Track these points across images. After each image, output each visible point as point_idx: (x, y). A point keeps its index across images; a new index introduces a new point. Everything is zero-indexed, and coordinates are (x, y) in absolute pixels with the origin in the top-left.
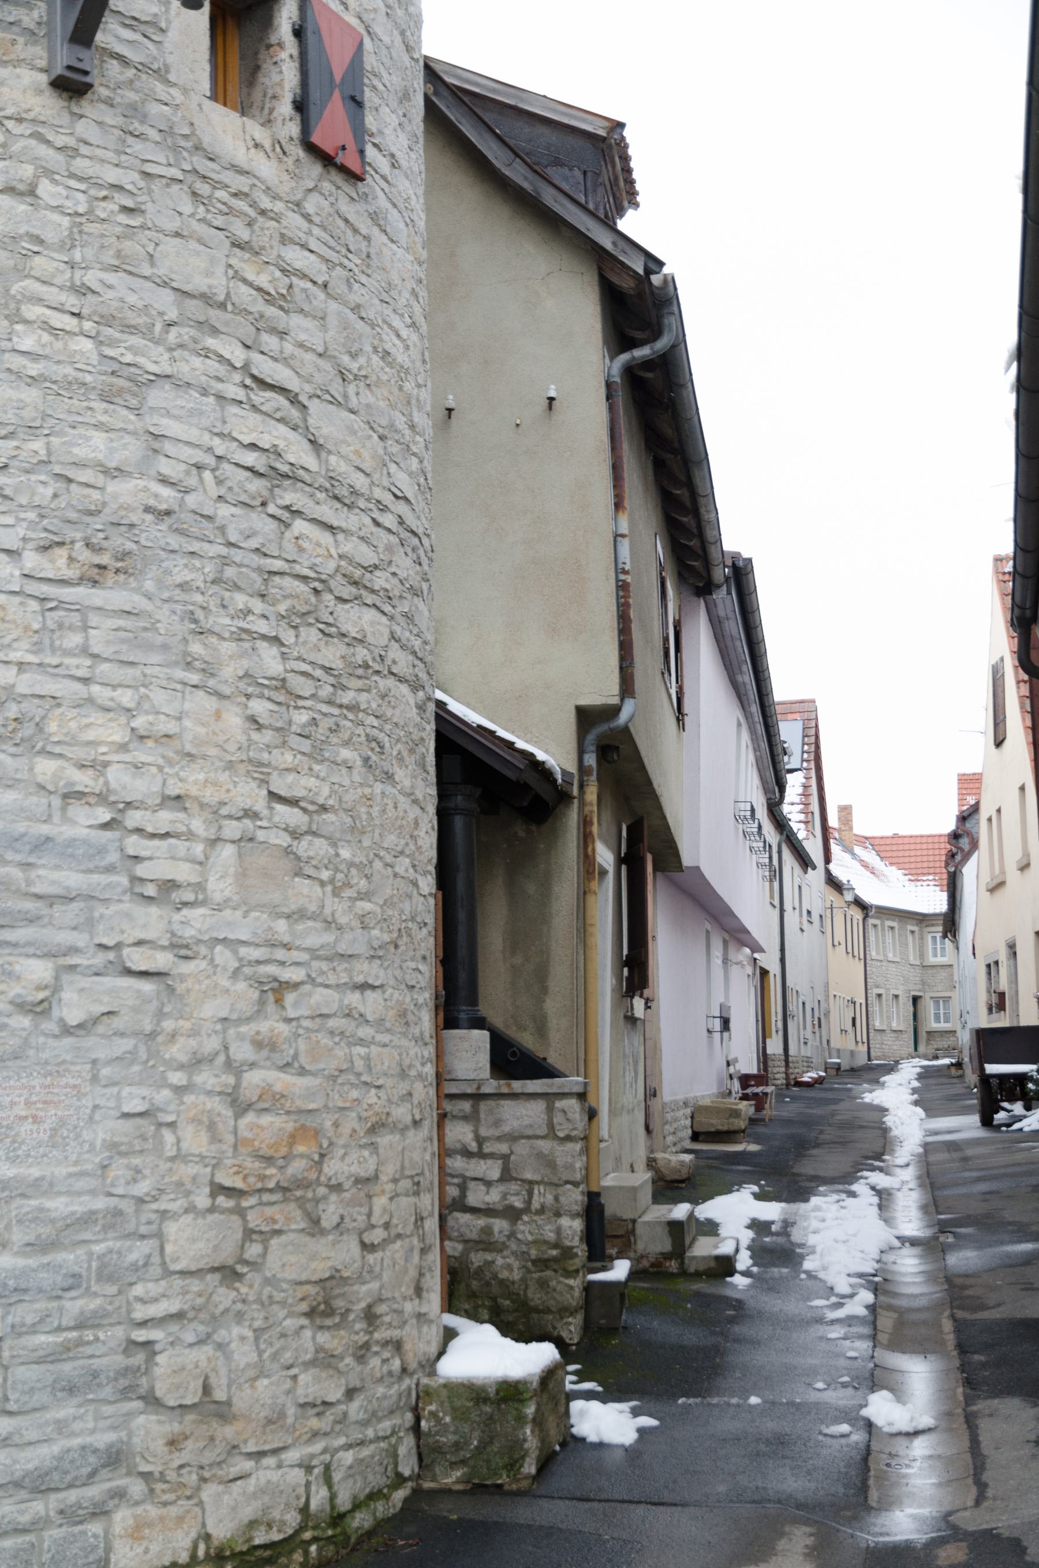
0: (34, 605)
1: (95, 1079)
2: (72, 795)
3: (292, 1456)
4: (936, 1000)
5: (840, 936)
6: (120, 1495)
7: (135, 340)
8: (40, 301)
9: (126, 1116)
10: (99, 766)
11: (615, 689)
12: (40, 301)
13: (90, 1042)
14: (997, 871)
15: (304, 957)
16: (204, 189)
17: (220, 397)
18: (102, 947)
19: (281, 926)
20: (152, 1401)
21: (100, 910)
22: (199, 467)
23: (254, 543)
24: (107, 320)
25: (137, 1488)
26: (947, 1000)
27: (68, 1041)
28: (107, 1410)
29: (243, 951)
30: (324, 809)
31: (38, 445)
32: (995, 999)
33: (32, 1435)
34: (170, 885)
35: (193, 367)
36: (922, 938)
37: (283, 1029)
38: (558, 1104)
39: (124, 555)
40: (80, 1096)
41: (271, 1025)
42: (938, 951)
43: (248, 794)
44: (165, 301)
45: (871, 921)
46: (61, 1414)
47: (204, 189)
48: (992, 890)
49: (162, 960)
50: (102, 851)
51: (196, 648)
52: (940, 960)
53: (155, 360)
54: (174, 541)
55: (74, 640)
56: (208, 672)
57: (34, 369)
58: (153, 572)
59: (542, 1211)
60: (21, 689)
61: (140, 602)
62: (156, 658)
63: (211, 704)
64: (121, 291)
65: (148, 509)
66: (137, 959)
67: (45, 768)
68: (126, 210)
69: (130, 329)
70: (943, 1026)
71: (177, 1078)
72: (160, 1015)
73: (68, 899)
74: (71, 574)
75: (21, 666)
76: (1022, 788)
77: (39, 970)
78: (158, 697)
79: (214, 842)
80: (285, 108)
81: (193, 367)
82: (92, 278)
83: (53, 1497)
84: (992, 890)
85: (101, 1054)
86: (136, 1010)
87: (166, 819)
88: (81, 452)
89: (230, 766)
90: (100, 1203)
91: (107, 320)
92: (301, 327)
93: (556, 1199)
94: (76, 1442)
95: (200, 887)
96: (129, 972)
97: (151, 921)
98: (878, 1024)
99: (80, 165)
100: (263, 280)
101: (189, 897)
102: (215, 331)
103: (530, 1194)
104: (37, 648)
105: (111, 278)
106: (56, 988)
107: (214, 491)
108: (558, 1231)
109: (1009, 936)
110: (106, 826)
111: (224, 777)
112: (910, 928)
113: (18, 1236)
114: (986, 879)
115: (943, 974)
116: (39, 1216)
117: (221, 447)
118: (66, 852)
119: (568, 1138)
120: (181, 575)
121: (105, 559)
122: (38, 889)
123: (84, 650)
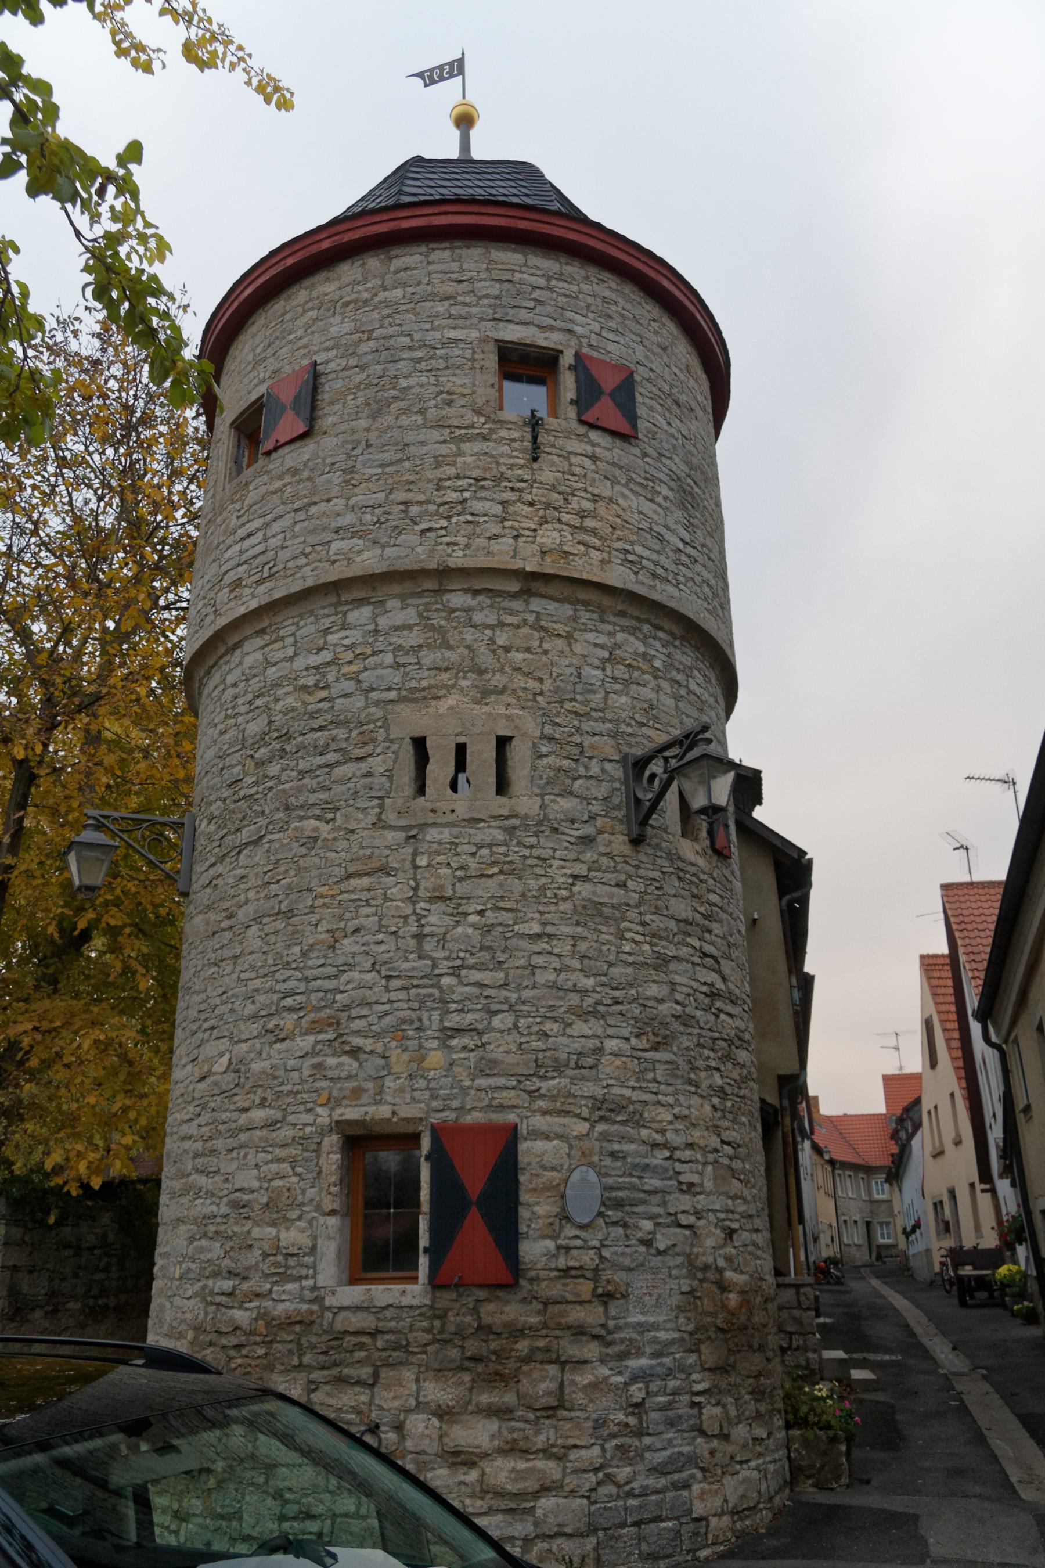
0: (636, 1061)
1: (670, 1276)
2: (655, 1145)
3: (753, 1464)
4: (881, 1224)
5: (821, 1182)
6: (692, 1477)
7: (664, 943)
8: (630, 930)
9: (683, 1293)
10: (663, 1132)
11: (797, 1066)
12: (630, 930)
13: (667, 1258)
14: (937, 1144)
15: (737, 1217)
16: (681, 874)
17: (693, 963)
18: (670, 1214)
19: (730, 1202)
20: (703, 1433)
21: (668, 1197)
22: (689, 995)
23: (708, 1026)
24: (653, 936)
25: (699, 1475)
26: (888, 1224)
27: (659, 1258)
28: (686, 1435)
29: (719, 1215)
30: (739, 1146)
31: (633, 992)
32: (942, 1226)
33: (659, 1446)
34: (691, 1185)
35: (684, 951)
36: (869, 1183)
37: (733, 1251)
38: (802, 1290)
39: (665, 1037)
40: (666, 1283)
41: (729, 1250)
42: (881, 1191)
43: (714, 1141)
44: (672, 925)
45: (837, 1172)
46: (670, 1435)
47: (681, 874)
48: (935, 1156)
49: (692, 1220)
50: (666, 1170)
51: (692, 1076)
52: (881, 1197)
53: (671, 951)
54: (682, 1029)
55: (650, 1076)
56: (697, 1087)
57: (630, 959)
58: (676, 1043)
59: (797, 1349)
60: (634, 1098)
61: (672, 1057)
62: (679, 1081)
63: (699, 1100)
64: (657, 922)
65: (673, 1016)
66: (684, 1219)
67: (644, 1133)
68: (657, 888)
69: (661, 938)
70: (886, 1241)
71: (700, 1275)
72: (692, 1246)
73: (655, 1192)
74: (648, 1046)
75: (633, 1088)
76: (952, 1095)
77: (647, 1225)
78: (682, 1098)
79: (705, 1164)
80: (704, 834)
81: (684, 951)
82: (648, 918)
83: (669, 1477)
84: (935, 1156)
85: (671, 1264)
86: (684, 1243)
87: (687, 1154)
88: (648, 993)
89: (707, 1128)
90: (676, 1335)
91: (653, 936)
92: (715, 926)
93: (805, 1341)
94: (676, 1450)
95: (702, 1185)
96: (680, 1226)
97: (685, 1202)
98: (845, 1240)
99: (641, 872)
100: (702, 910)
101: (698, 1190)
102: (689, 935)
103: (791, 1339)
104: (638, 1080)
105: (653, 917)
106: (654, 1233)
107: (694, 1004)
108: (807, 1360)
109: (950, 1185)
110: (667, 1159)
111: (706, 1133)
112: (848, 1173)
113: (648, 1350)
114: (928, 1149)
115: (884, 1206)
116: (655, 1341)
117: (694, 984)
118: (653, 1170)
119: (808, 1309)
120: (686, 1044)
121: (659, 1039)
122: (646, 1188)
123: (655, 1080)
